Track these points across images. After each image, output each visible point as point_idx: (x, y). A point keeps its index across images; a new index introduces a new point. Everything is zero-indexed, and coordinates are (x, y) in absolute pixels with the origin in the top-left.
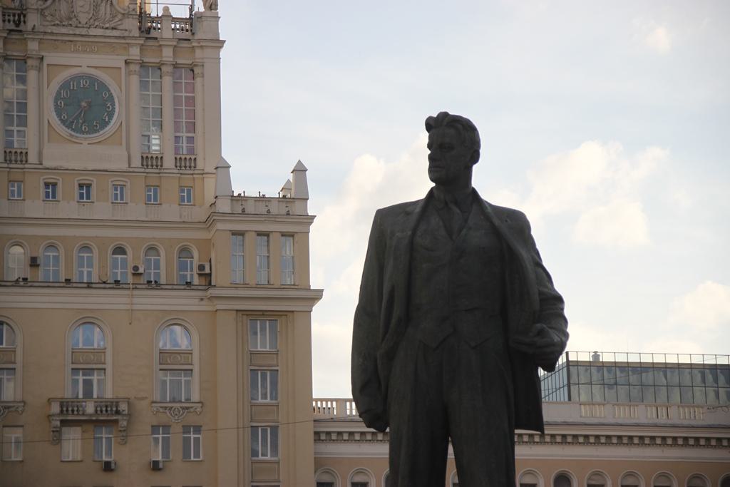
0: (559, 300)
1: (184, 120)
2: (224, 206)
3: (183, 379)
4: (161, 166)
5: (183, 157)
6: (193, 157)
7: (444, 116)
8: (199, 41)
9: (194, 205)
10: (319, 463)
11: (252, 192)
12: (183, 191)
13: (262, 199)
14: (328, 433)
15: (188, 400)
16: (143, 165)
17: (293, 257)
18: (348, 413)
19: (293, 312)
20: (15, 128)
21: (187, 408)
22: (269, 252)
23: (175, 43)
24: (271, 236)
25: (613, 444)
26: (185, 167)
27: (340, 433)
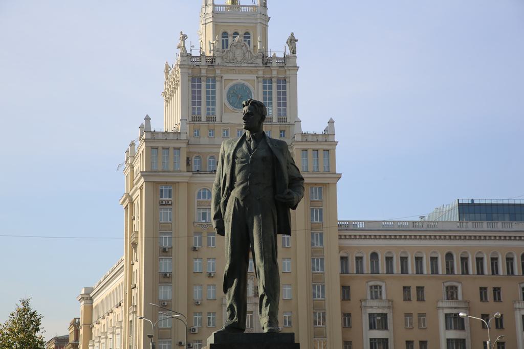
10: (341, 248)
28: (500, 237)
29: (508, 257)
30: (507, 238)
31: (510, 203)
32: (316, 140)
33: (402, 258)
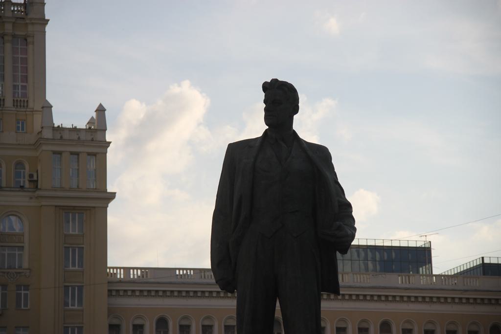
0: (349, 206)
1: (20, 74)
2: (48, 134)
3: (17, 253)
4: (27, 106)
5: (19, 99)
6: (26, 100)
7: (275, 81)
8: (31, 19)
9: (26, 133)
10: (111, 311)
11: (67, 124)
12: (18, 123)
13: (74, 130)
14: (118, 291)
15: (20, 267)
16: (14, 106)
17: (95, 170)
18: (132, 277)
19: (94, 207)
20: (20, 84)
21: (20, 273)
22: (78, 166)
23: (14, 20)
24: (80, 155)
25: (213, 297)
26: (20, 106)
27: (125, 291)
28: (350, 295)
29: (361, 327)
30: (361, 298)
31: (394, 245)
32: (89, 138)
33: (181, 327)
